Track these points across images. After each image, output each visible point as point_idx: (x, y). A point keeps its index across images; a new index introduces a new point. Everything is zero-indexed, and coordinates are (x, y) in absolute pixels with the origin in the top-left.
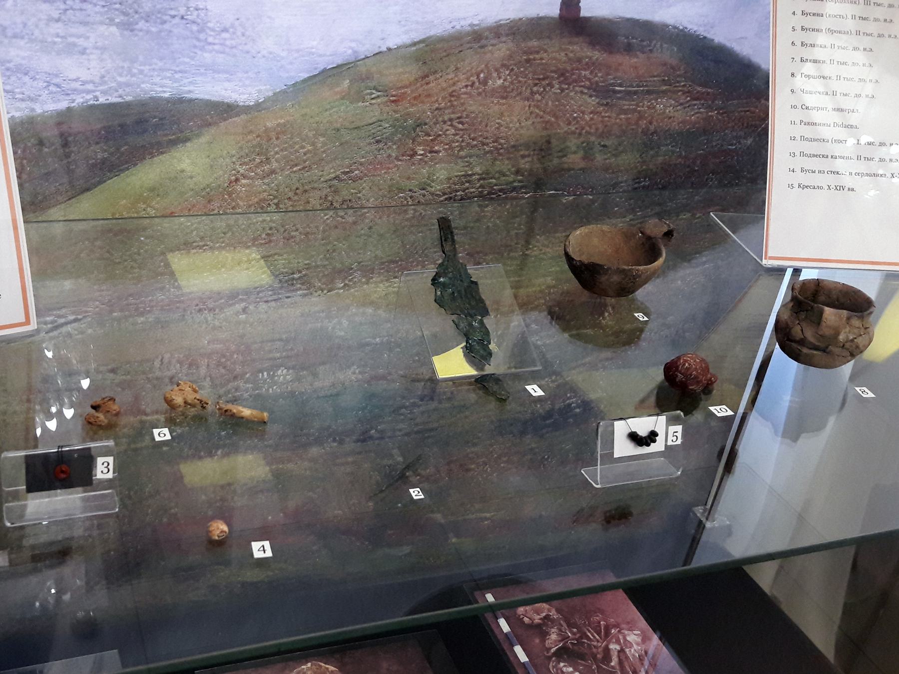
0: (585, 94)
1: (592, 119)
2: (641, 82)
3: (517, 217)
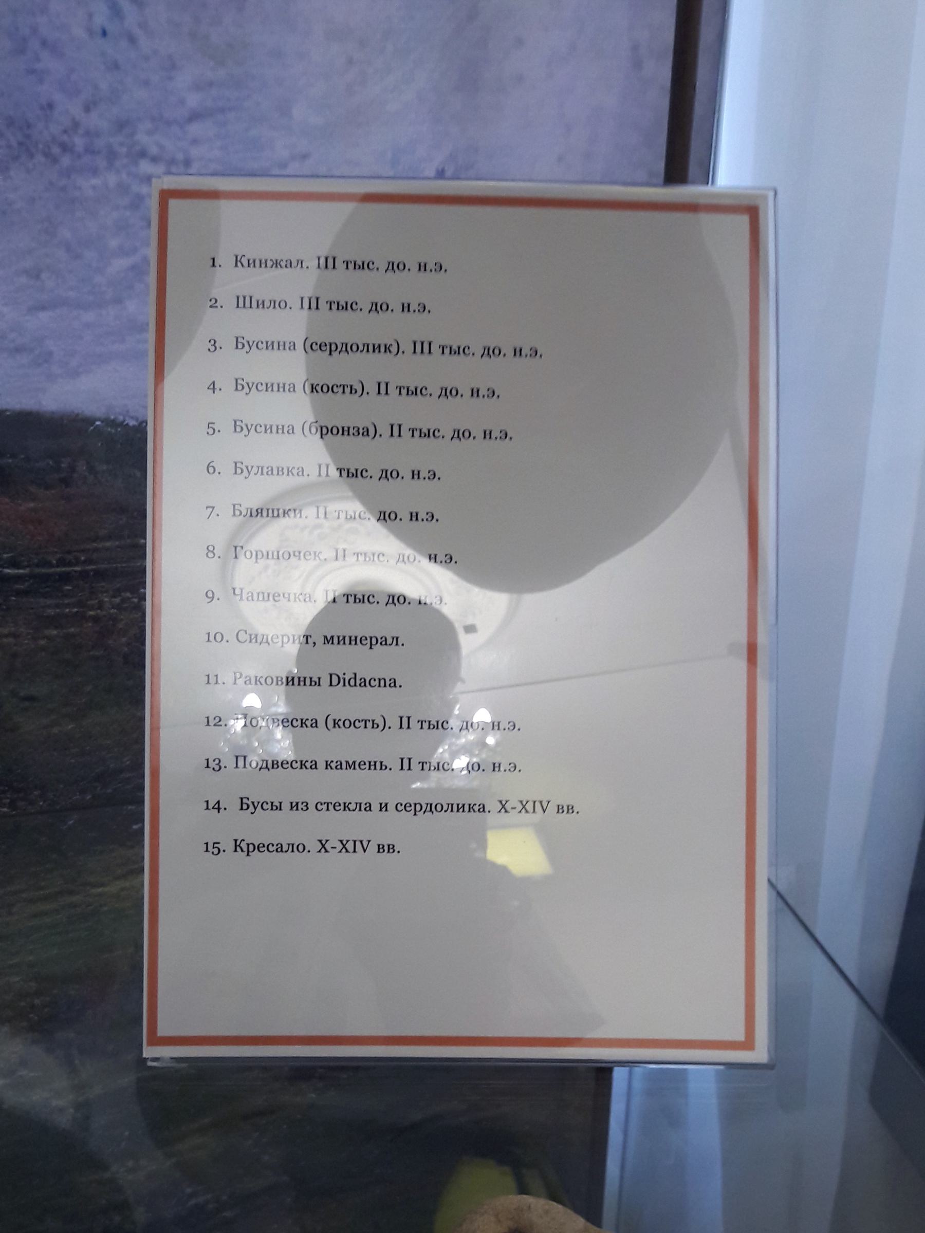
2: (69, 552)
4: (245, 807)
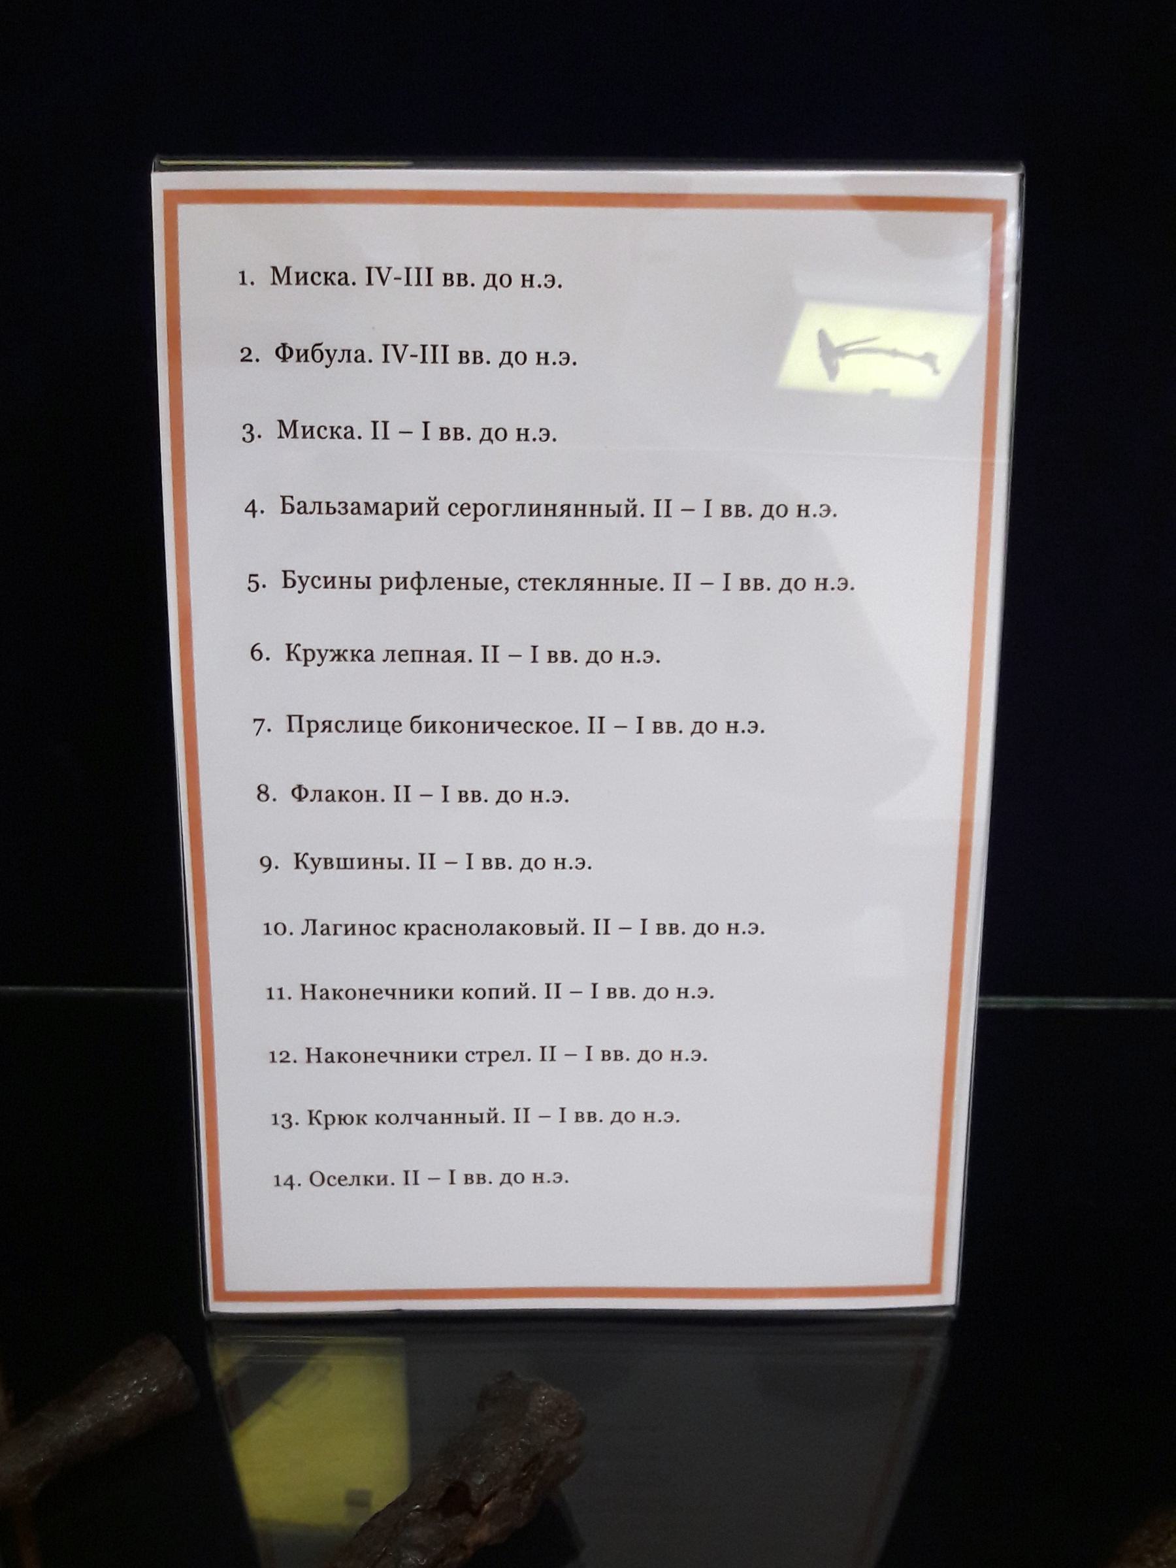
4: (290, 583)
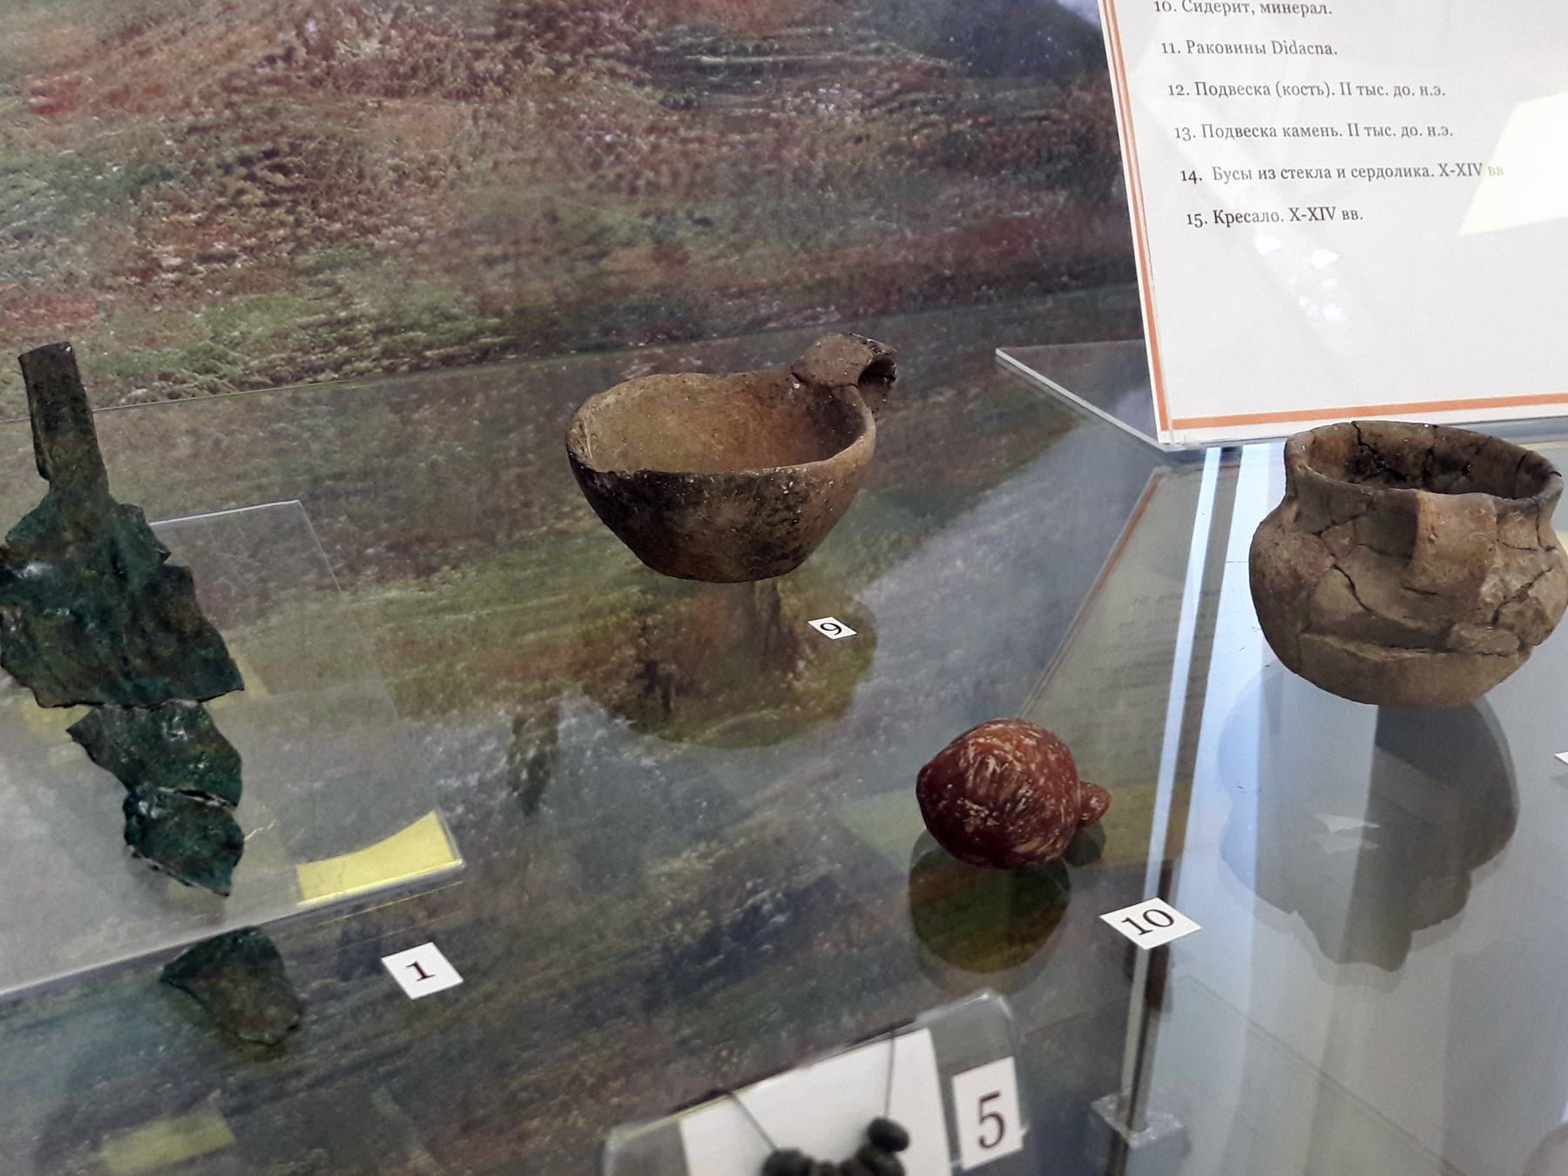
0: (623, 77)
1: (655, 148)
2: (765, 39)
3: (509, 431)
